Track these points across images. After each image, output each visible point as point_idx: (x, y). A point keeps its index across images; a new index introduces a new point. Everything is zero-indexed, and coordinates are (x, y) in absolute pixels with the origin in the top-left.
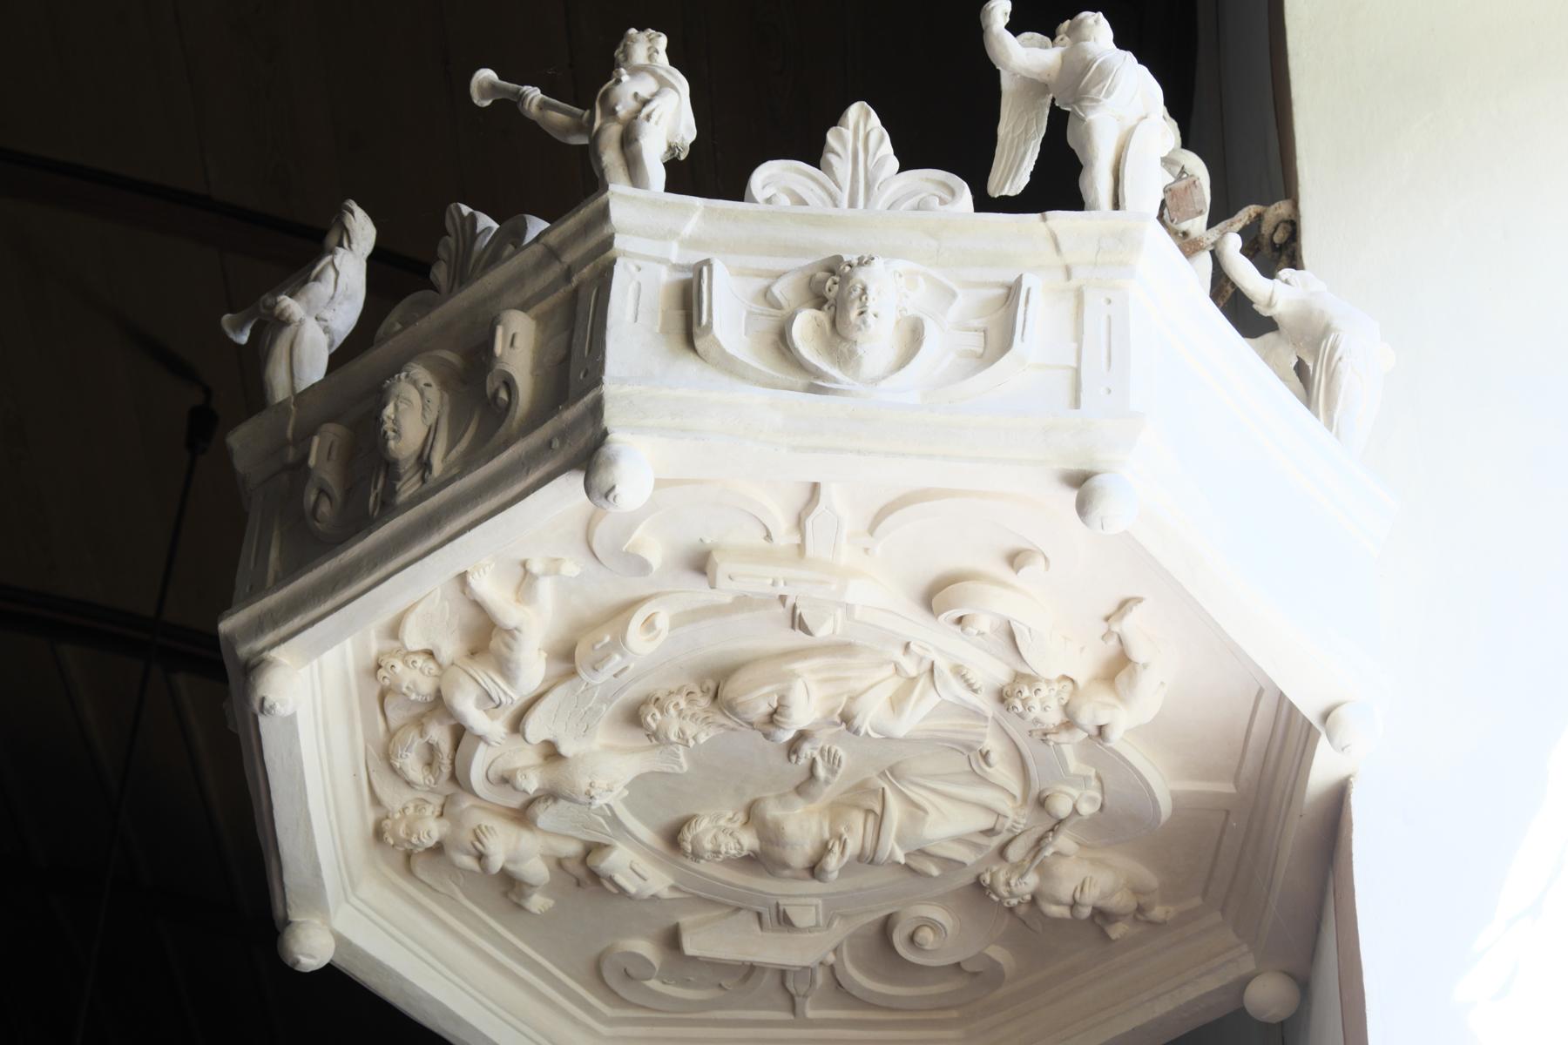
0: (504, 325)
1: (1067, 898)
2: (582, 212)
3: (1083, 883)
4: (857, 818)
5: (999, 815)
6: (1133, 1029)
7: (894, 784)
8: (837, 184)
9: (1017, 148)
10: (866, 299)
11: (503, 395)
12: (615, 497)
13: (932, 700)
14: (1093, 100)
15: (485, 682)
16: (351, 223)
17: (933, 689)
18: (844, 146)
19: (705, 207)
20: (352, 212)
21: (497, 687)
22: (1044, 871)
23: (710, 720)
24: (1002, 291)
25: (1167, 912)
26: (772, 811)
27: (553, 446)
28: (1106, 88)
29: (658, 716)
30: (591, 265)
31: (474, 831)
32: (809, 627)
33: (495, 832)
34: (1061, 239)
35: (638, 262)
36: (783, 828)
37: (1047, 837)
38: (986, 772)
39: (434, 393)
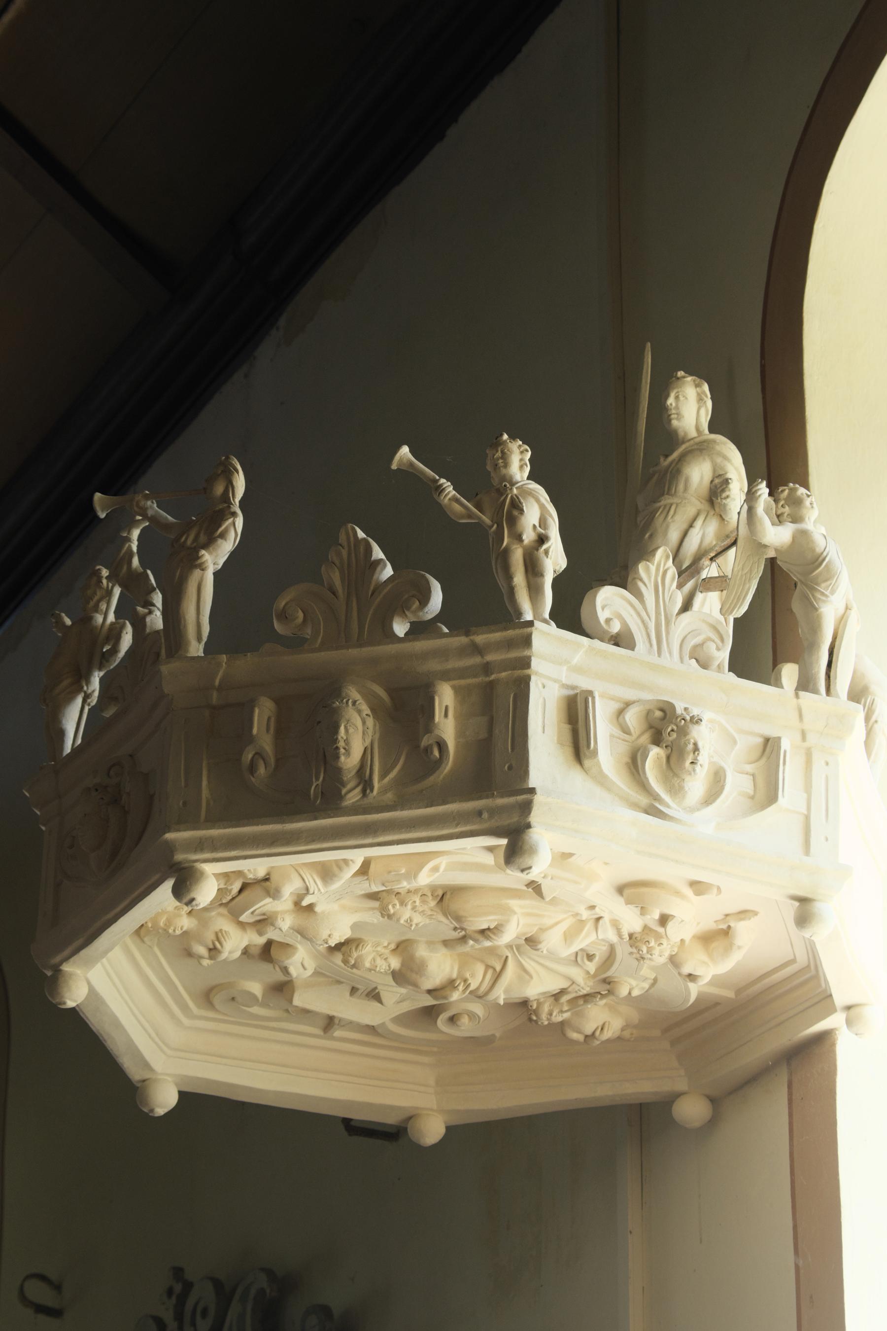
0: (439, 696)
1: (589, 1030)
2: (508, 632)
3: (604, 1024)
4: (480, 969)
5: (573, 983)
6: (576, 1099)
7: (515, 954)
8: (650, 619)
9: (744, 584)
10: (698, 754)
11: (436, 753)
12: (529, 873)
13: (593, 937)
14: (823, 594)
15: (309, 882)
16: (237, 481)
17: (595, 933)
18: (649, 577)
19: (589, 646)
20: (238, 473)
21: (316, 886)
22: (579, 1014)
23: (434, 917)
24: (760, 740)
25: (632, 1034)
26: (421, 952)
27: (483, 817)
28: (832, 585)
29: (398, 906)
30: (510, 672)
31: (217, 934)
32: (544, 895)
33: (231, 938)
34: (804, 712)
35: (545, 681)
36: (427, 966)
37: (595, 997)
38: (584, 963)
39: (370, 722)
